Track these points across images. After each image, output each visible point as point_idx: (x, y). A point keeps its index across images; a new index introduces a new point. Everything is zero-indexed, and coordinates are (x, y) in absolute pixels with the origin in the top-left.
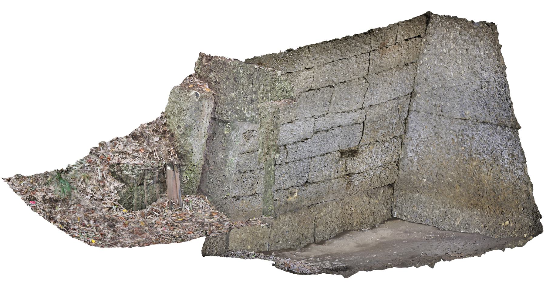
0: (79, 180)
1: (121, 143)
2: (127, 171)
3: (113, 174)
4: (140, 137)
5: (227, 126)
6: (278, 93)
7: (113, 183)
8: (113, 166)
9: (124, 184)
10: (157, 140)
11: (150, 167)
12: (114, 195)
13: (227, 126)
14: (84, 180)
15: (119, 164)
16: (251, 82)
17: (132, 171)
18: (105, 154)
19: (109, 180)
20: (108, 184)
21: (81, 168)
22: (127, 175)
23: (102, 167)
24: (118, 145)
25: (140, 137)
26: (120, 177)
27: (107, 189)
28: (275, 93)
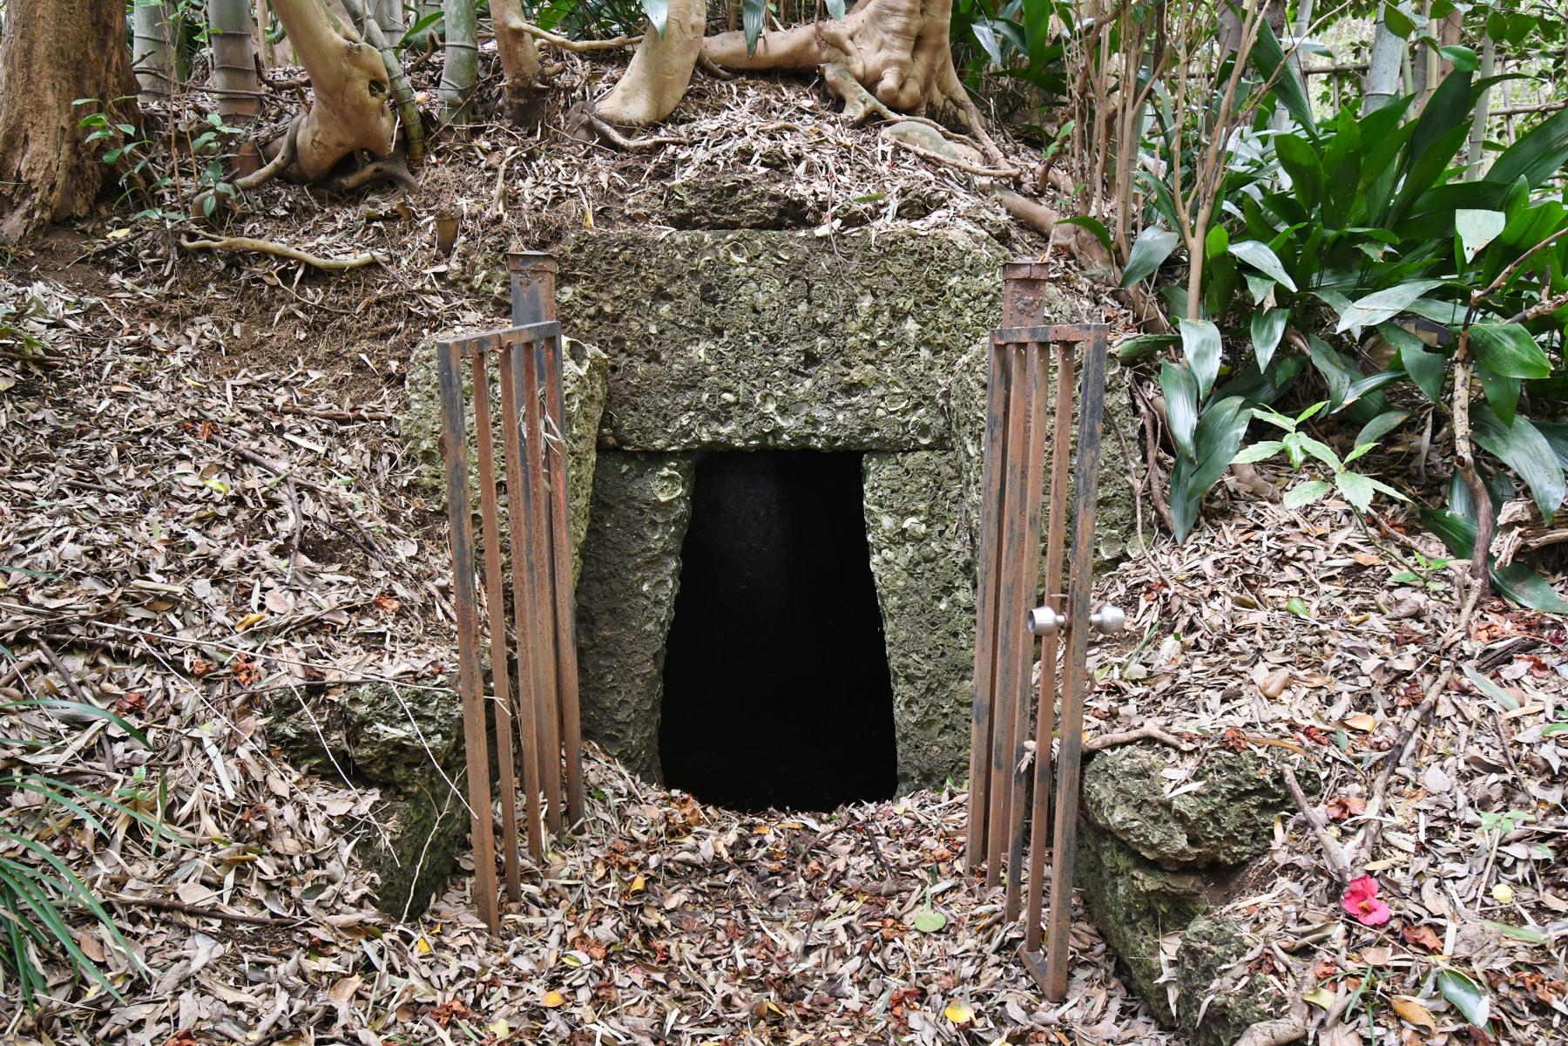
0: (102, 841)
1: (269, 582)
2: (390, 720)
3: (299, 750)
4: (339, 546)
5: (666, 472)
6: (958, 313)
7: (312, 801)
8: (285, 707)
9: (374, 795)
10: (413, 550)
11: (1522, 956)
12: (351, 882)
13: (666, 472)
14: (134, 830)
15: (316, 688)
16: (802, 291)
17: (418, 718)
18: (207, 647)
19: (282, 789)
20: (290, 814)
21: (88, 753)
22: (398, 746)
23: (221, 725)
24: (256, 593)
25: (339, 546)
26: (343, 757)
27: (288, 844)
28: (945, 317)
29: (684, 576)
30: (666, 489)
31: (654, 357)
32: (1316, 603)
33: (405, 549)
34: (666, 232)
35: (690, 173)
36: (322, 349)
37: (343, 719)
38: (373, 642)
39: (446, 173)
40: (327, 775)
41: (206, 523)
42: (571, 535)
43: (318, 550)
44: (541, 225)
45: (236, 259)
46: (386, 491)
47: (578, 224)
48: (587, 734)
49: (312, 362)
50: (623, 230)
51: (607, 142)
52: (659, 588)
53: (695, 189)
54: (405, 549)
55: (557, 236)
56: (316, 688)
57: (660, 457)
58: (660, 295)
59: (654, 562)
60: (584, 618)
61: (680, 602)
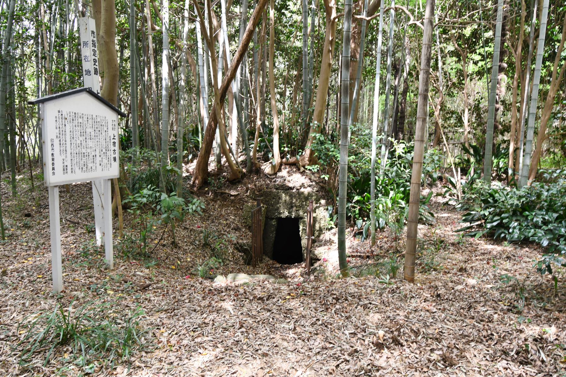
3: (237, 249)
8: (235, 244)
29: (276, 234)
30: (274, 223)
31: (273, 206)
32: (458, 304)
33: (244, 230)
34: (275, 190)
35: (278, 183)
36: (233, 205)
37: (240, 246)
38: (242, 239)
39: (247, 181)
40: (240, 252)
41: (225, 226)
42: (262, 228)
43: (236, 230)
44: (259, 189)
45: (222, 193)
46: (241, 223)
47: (264, 189)
48: (264, 253)
49: (232, 207)
50: (269, 190)
51: (267, 177)
52: (273, 235)
53: (278, 185)
54: (244, 230)
55: (261, 190)
56: (238, 243)
57: (273, 219)
58: (273, 198)
59: (273, 232)
60: (264, 239)
61: (276, 237)
